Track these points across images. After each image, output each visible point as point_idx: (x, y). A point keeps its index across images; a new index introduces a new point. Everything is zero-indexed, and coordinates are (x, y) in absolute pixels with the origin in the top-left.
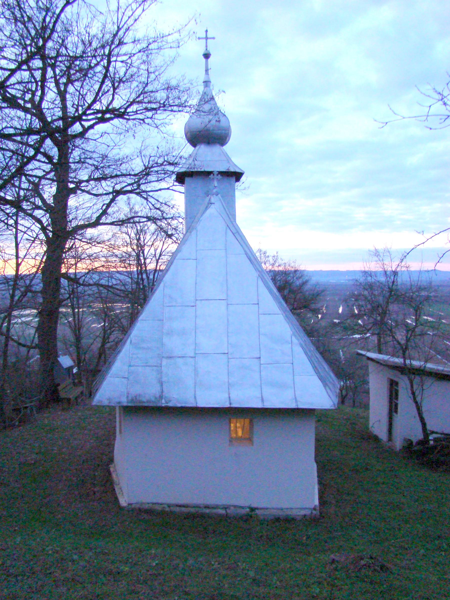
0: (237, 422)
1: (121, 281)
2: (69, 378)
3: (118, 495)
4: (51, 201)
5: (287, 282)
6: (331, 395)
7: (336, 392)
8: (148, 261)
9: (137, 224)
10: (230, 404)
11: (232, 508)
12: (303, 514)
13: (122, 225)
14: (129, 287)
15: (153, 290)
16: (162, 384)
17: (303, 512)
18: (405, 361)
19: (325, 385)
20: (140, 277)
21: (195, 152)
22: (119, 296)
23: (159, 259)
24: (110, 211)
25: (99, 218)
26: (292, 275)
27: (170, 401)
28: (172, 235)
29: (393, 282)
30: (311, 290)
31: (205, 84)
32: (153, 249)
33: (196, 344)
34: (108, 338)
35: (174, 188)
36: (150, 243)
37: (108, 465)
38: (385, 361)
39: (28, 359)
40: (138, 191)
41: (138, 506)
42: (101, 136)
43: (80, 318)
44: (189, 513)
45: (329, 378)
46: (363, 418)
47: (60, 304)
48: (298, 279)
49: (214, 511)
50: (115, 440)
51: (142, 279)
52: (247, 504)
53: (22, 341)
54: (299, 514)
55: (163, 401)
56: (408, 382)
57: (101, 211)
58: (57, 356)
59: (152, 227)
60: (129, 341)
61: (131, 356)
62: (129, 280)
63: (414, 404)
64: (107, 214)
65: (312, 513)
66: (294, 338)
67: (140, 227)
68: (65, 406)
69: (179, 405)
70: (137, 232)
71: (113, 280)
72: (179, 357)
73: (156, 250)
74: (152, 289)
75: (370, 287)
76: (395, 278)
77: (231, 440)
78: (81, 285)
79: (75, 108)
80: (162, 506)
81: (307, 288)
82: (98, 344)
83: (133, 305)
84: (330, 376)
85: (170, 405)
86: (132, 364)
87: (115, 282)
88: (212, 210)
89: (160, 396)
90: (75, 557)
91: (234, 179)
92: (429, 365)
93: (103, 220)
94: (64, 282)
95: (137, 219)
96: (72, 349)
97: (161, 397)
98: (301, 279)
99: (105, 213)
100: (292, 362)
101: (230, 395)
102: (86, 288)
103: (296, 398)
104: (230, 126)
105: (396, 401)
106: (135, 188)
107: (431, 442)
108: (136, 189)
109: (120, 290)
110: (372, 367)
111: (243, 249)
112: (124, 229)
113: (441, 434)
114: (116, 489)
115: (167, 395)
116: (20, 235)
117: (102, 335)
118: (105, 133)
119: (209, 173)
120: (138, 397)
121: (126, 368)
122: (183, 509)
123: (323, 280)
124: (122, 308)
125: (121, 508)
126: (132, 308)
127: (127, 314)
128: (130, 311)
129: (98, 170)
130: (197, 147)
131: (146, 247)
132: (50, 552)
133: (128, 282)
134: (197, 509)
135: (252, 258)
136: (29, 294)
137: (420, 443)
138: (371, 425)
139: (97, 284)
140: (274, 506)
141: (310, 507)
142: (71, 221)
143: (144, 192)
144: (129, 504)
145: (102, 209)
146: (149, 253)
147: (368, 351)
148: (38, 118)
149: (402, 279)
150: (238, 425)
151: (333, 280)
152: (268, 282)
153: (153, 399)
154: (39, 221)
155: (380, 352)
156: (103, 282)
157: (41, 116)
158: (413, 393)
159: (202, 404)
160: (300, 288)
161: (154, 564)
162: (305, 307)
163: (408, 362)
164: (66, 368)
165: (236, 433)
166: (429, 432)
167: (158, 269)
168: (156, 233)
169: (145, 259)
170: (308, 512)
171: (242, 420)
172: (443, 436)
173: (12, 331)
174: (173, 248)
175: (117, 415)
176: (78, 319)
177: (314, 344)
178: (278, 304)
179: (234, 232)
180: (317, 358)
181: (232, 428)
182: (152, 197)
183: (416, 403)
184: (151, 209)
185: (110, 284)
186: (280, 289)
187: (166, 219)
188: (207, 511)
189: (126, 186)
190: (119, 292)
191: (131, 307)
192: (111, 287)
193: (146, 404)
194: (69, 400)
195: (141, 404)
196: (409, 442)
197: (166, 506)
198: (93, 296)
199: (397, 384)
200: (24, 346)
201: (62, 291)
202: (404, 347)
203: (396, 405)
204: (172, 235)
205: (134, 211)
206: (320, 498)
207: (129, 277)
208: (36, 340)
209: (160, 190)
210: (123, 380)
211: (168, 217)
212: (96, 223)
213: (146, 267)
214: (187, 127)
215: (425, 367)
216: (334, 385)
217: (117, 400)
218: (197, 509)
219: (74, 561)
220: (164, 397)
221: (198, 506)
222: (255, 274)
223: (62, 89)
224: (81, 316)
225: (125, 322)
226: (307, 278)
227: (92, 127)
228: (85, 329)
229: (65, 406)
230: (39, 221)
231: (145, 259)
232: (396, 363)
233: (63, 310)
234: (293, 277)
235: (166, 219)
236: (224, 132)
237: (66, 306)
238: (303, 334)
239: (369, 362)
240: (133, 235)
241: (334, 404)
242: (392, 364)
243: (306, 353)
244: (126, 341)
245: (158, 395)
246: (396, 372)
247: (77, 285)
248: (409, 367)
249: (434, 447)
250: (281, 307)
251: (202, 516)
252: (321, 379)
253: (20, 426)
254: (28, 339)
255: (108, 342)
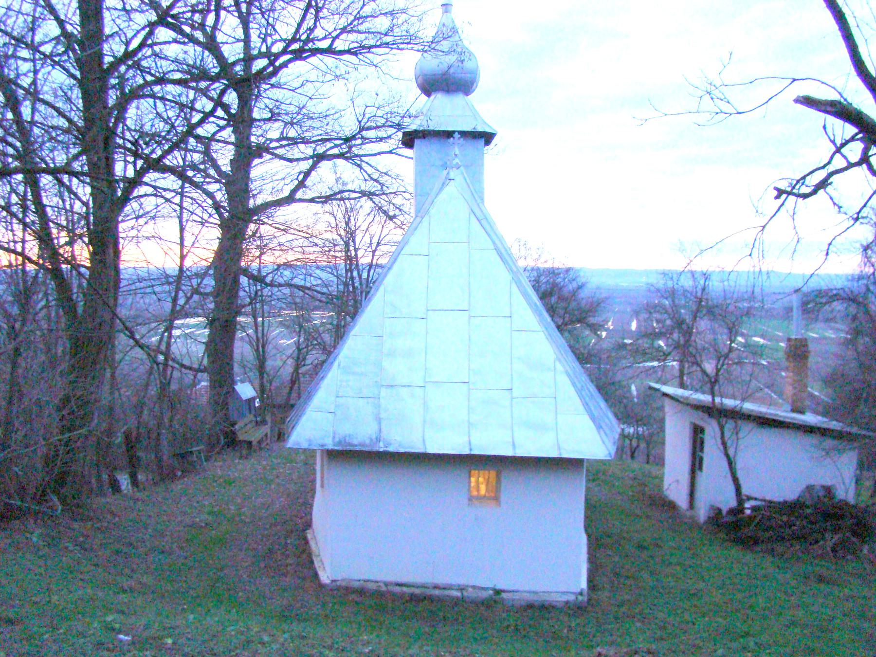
0: (479, 477)
1: (323, 281)
2: (250, 412)
3: (318, 569)
4: (226, 168)
5: (555, 285)
6: (606, 440)
7: (614, 438)
8: (360, 253)
9: (346, 201)
10: (471, 450)
11: (470, 589)
12: (566, 600)
13: (325, 202)
14: (333, 289)
15: (370, 295)
16: (380, 423)
17: (565, 598)
18: (713, 400)
19: (599, 427)
20: (349, 274)
21: (429, 104)
22: (321, 301)
23: (376, 250)
24: (308, 182)
25: (294, 191)
26: (562, 275)
27: (391, 444)
28: (395, 216)
29: (703, 289)
30: (589, 298)
31: (444, 7)
32: (367, 235)
33: (426, 369)
34: (304, 359)
35: (399, 151)
36: (364, 227)
37: (304, 531)
38: (687, 398)
39: (194, 385)
40: (349, 155)
41: (344, 584)
42: (302, 85)
43: (265, 331)
44: (412, 594)
45: (607, 420)
46: (655, 477)
47: (239, 313)
48: (570, 282)
49: (447, 592)
50: (313, 497)
51: (352, 278)
52: (491, 586)
53: (186, 362)
54: (560, 599)
55: (381, 444)
56: (717, 429)
57: (296, 182)
58: (234, 383)
59: (366, 205)
60: (336, 364)
61: (339, 384)
62: (335, 279)
63: (725, 459)
64: (305, 186)
65: (577, 598)
66: (557, 363)
67: (351, 205)
68: (244, 452)
69: (402, 450)
70: (347, 211)
71: (312, 278)
72: (404, 386)
73: (371, 238)
74: (368, 293)
75: (672, 293)
76: (707, 283)
77: (471, 499)
78: (267, 285)
79: (261, 38)
80: (377, 584)
81: (583, 294)
82: (289, 369)
83: (338, 314)
84: (608, 418)
85: (391, 449)
86: (340, 395)
87: (314, 283)
88: (451, 189)
89: (377, 438)
90: (266, 638)
91: (482, 142)
92: (749, 406)
93: (299, 195)
94: (244, 280)
95: (346, 195)
96: (254, 374)
97: (378, 440)
98: (575, 282)
99: (302, 184)
100: (554, 396)
101: (471, 438)
102: (275, 289)
103: (558, 445)
104: (478, 67)
105: (700, 454)
106: (345, 150)
107: (748, 512)
108: (347, 153)
109: (323, 294)
110: (668, 405)
111: (492, 240)
112: (327, 207)
113: (761, 500)
114: (315, 562)
115: (385, 437)
116: (185, 215)
117: (295, 355)
118: (307, 81)
119: (449, 134)
120: (347, 439)
121: (333, 398)
122: (405, 589)
123: (608, 282)
124: (323, 318)
125: (321, 586)
126: (338, 318)
127: (329, 326)
128: (335, 323)
129: (292, 126)
130: (432, 97)
131: (357, 232)
132: (233, 633)
133: (332, 281)
134: (423, 590)
135: (504, 253)
136: (196, 297)
137: (732, 512)
138: (666, 485)
139: (288, 285)
140: (526, 588)
141: (575, 591)
142: (254, 196)
143: (357, 156)
144: (333, 581)
145: (297, 179)
146: (363, 242)
147: (664, 384)
148: (209, 50)
149: (715, 285)
150: (481, 479)
151: (624, 283)
152: (526, 286)
153: (368, 441)
154: (211, 195)
155: (682, 385)
156: (298, 281)
157: (212, 46)
158: (724, 444)
159: (432, 449)
160: (574, 295)
161: (367, 650)
162: (579, 321)
163: (717, 400)
164: (246, 400)
165: (478, 490)
166: (744, 498)
167: (374, 262)
168: (373, 213)
169: (356, 250)
170: (571, 598)
171: (487, 472)
172: (763, 503)
173: (174, 348)
174: (397, 235)
175: (318, 468)
176: (263, 334)
177: (590, 375)
178: (537, 317)
179: (480, 218)
180: (589, 391)
181: (473, 484)
182: (367, 163)
183: (727, 455)
184: (366, 180)
185: (308, 285)
186: (544, 296)
187: (386, 194)
188: (437, 592)
189: (331, 148)
190: (319, 295)
191: (335, 317)
192: (309, 289)
193: (358, 448)
194: (250, 443)
195: (352, 448)
196: (717, 511)
197: (382, 585)
198: (284, 301)
199: (702, 430)
200: (190, 368)
201: (242, 294)
202: (713, 380)
203: (701, 460)
204: (395, 216)
205: (341, 181)
206: (590, 580)
207: (333, 274)
208: (205, 362)
209: (380, 154)
210: (328, 414)
211: (388, 191)
212: (290, 199)
213: (357, 261)
214: (418, 67)
215: (741, 407)
216: (611, 428)
217: (321, 442)
218: (423, 590)
219: (264, 644)
220: (382, 439)
221: (424, 586)
222: (506, 276)
223: (244, 10)
224: (266, 329)
225: (327, 337)
226: (583, 280)
227: (285, 65)
228: (271, 347)
229: (244, 452)
230: (211, 195)
231: (356, 250)
232: (700, 401)
233: (241, 319)
234: (564, 279)
235: (386, 194)
236: (469, 75)
237: (246, 315)
238: (571, 357)
239: (667, 401)
240: (340, 216)
241: (610, 454)
242: (695, 403)
243: (574, 384)
244: (332, 363)
245: (374, 437)
246: (700, 413)
247: (261, 286)
248: (719, 406)
249: (751, 518)
250: (541, 320)
251: (430, 599)
252: (593, 419)
253: (184, 477)
254: (194, 359)
255: (304, 365)
